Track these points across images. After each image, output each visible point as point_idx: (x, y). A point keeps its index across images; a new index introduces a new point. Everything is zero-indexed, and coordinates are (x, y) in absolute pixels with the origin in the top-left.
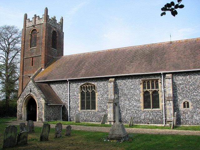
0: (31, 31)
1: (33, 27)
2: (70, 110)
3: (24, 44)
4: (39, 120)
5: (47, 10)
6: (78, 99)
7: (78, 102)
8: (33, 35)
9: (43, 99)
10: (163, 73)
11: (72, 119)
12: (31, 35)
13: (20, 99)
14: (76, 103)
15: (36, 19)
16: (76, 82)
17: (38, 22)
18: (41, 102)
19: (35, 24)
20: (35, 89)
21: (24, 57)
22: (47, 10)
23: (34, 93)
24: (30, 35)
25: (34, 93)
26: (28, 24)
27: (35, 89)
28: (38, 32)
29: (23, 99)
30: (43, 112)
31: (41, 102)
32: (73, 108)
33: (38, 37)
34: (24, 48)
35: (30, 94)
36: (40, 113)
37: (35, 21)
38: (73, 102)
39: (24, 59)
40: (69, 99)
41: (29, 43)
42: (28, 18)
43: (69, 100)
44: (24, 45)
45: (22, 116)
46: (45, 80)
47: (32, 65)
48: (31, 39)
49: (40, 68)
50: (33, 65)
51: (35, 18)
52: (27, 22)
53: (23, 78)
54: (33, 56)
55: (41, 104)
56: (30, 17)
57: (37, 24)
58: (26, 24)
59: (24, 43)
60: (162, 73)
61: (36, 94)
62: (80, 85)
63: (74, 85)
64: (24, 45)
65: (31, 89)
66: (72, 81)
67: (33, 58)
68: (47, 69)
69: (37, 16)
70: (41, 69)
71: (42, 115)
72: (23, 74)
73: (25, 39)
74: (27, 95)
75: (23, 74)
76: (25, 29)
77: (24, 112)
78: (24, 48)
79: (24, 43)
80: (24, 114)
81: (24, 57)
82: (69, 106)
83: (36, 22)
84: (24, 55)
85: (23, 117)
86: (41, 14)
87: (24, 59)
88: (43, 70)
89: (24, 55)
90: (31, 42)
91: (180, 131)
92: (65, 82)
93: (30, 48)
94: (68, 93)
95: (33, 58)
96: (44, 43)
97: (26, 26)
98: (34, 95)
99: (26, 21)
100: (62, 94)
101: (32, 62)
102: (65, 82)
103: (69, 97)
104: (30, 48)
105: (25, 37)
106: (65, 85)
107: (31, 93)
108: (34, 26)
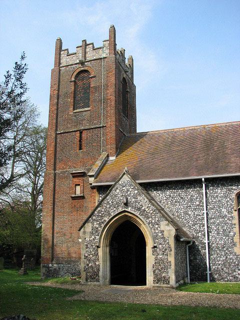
0: (75, 73)
1: (80, 66)
2: (209, 253)
3: (58, 102)
4: (158, 280)
5: (113, 31)
6: (232, 224)
7: (232, 233)
8: (80, 83)
9: (168, 225)
10: (205, 179)
11: (216, 277)
12: (74, 81)
13: (90, 224)
14: (228, 236)
15: (88, 50)
16: (223, 185)
17: (91, 55)
18: (162, 232)
19: (85, 59)
20: (139, 198)
21: (56, 130)
22: (113, 31)
23: (139, 209)
24: (73, 83)
25: (139, 209)
26: (65, 60)
27: (139, 198)
28: (95, 77)
29: (100, 224)
30: (172, 259)
31: (162, 232)
32: (218, 248)
33: (95, 88)
34: (57, 110)
35: (125, 211)
36: (158, 262)
37: (85, 53)
38: (218, 233)
39: (56, 133)
40: (206, 227)
41: (70, 100)
42: (63, 48)
43: (208, 227)
44: (58, 105)
45: (99, 270)
46: (187, 175)
47: (80, 149)
48: (75, 91)
49: (104, 155)
50: (83, 147)
51: (86, 48)
52: (62, 56)
53: (55, 177)
54: (82, 128)
55: (164, 238)
56: (71, 45)
57: (88, 59)
58: (60, 59)
59: (58, 99)
60: (203, 180)
61: (144, 210)
62: (236, 192)
63: (220, 191)
64: (58, 105)
65: (127, 199)
66: (211, 182)
67: (81, 133)
68: (123, 156)
69: (88, 43)
70: (108, 156)
71: (166, 268)
72: (55, 170)
73: (58, 91)
74: (113, 214)
75: (55, 170)
76: (60, 70)
77: (104, 261)
78: (57, 110)
79: (58, 99)
80: (104, 265)
81: (56, 130)
82: (209, 243)
83: (87, 55)
84: (57, 127)
85: (101, 274)
86: (99, 38)
87: (57, 134)
88: (112, 158)
89: (57, 127)
90: (74, 97)
91: (204, 295)
92: (196, 183)
93: (74, 109)
94: (205, 211)
95: (81, 133)
96: (113, 98)
97: (60, 63)
98: (137, 213)
99: (60, 54)
100: (186, 213)
101: (80, 141)
102: (196, 183)
103: (207, 221)
104: (74, 109)
105: (59, 86)
106: (192, 192)
107: (129, 209)
108: (82, 63)
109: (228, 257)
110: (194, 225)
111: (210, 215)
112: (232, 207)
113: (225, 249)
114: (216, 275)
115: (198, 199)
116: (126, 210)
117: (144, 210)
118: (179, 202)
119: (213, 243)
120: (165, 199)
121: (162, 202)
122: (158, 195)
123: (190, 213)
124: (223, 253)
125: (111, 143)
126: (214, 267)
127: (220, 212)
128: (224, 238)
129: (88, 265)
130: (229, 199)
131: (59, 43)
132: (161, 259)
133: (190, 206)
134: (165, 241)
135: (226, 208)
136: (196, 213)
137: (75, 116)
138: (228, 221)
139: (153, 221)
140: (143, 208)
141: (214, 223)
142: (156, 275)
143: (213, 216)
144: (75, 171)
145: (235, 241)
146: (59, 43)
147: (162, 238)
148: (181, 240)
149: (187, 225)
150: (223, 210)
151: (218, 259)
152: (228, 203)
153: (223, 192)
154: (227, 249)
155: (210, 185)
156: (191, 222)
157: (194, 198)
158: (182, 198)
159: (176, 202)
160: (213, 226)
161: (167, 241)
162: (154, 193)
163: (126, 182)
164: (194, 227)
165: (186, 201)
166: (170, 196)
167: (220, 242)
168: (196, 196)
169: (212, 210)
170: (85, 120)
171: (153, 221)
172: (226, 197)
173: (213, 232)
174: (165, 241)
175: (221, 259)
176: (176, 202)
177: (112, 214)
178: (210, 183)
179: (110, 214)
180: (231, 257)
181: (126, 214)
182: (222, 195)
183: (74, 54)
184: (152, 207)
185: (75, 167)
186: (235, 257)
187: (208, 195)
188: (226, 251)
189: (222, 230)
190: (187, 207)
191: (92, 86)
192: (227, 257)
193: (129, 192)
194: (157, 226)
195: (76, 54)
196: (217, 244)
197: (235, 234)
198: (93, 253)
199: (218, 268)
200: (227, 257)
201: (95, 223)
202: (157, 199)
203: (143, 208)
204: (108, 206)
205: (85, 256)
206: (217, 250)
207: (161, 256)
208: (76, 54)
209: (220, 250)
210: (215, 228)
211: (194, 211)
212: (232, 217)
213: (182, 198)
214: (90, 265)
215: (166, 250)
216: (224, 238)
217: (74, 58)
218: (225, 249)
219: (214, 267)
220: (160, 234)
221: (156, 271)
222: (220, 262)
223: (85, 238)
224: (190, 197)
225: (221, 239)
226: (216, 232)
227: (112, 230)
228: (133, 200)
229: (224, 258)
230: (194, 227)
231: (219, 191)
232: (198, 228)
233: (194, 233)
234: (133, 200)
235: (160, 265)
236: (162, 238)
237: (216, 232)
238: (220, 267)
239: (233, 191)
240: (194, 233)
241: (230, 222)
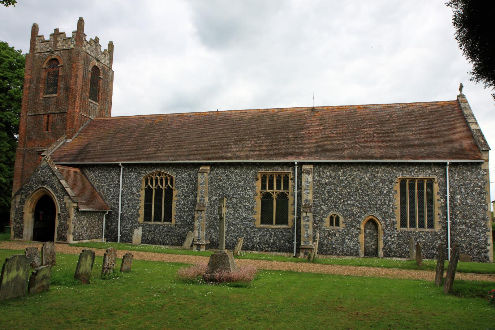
7: (138, 207)
14: (135, 209)
18: (65, 204)
26: (38, 46)
31: (65, 204)
32: (127, 217)
33: (63, 76)
38: (129, 207)
56: (46, 32)
67: (48, 116)
95: (48, 116)
100: (108, 189)
109: (134, 225)
110: (113, 199)
111: (124, 192)
112: (140, 187)
113: (132, 219)
114: (124, 237)
115: (117, 180)
116: (43, 186)
117: (55, 187)
118: (104, 181)
119: (124, 214)
120: (95, 177)
121: (93, 180)
122: (90, 174)
123: (111, 190)
124: (130, 222)
125: (70, 127)
126: (123, 232)
127: (132, 190)
128: (132, 210)
129: (16, 226)
130: (138, 181)
131: (35, 28)
132: (63, 223)
133: (111, 184)
134: (66, 211)
135: (136, 187)
136: (115, 190)
137: (44, 101)
138: (136, 198)
139: (60, 196)
140: (55, 186)
141: (126, 198)
142: (58, 234)
143: (126, 193)
144: (41, 149)
145: (139, 213)
146: (35, 28)
147: (64, 208)
148: (80, 210)
149: (108, 199)
150: (134, 189)
151: (127, 226)
152: (138, 184)
153: (135, 175)
154: (134, 219)
155: (126, 169)
156: (111, 197)
157: (115, 178)
158: (106, 178)
159: (102, 180)
160: (126, 201)
161: (68, 211)
162: (87, 172)
163: (45, 166)
164: (113, 201)
165: (109, 181)
166: (98, 176)
167: (129, 213)
168: (116, 177)
169: (126, 189)
170: (52, 105)
171: (60, 196)
172: (136, 179)
173: (125, 205)
174: (66, 211)
175: (129, 226)
176: (102, 180)
177: (34, 189)
178: (126, 167)
179: (33, 189)
180: (136, 224)
181: (44, 189)
182: (134, 177)
183: (47, 42)
184: (60, 185)
185: (41, 146)
186: (139, 225)
187: (125, 177)
188: (133, 220)
189: (131, 204)
190: (109, 185)
191: (60, 74)
192: (133, 225)
193: (46, 174)
194: (62, 199)
195: (48, 41)
196: (127, 215)
197: (140, 207)
198: (20, 217)
199: (126, 232)
200: (133, 225)
201: (23, 195)
202: (89, 178)
203: (55, 186)
204: (32, 183)
205: (14, 219)
206: (127, 219)
207: (63, 221)
208: (48, 41)
209: (129, 219)
210: (127, 203)
211: (114, 189)
212: (139, 194)
213: (106, 178)
214: (17, 226)
215: (66, 217)
216: (132, 210)
217: (47, 45)
218: (132, 219)
219: (123, 232)
220: (64, 205)
221: (59, 232)
222: (128, 228)
223: (16, 206)
224: (112, 177)
225: (130, 211)
226: (127, 206)
227: (36, 204)
228: (49, 179)
229: (131, 226)
230: (113, 201)
231: (132, 174)
232: (115, 202)
233: (112, 205)
234: (49, 179)
235: (62, 228)
236: (64, 208)
237: (127, 206)
238: (127, 232)
239: (142, 174)
240: (112, 205)
241: (138, 199)
